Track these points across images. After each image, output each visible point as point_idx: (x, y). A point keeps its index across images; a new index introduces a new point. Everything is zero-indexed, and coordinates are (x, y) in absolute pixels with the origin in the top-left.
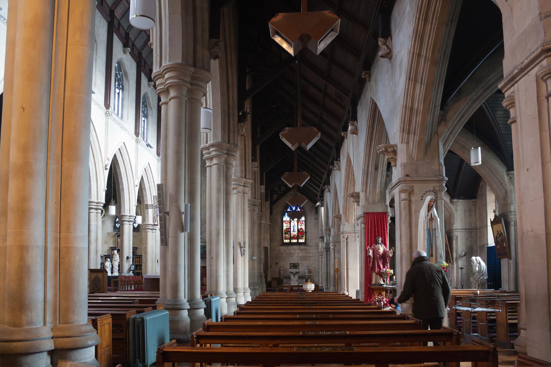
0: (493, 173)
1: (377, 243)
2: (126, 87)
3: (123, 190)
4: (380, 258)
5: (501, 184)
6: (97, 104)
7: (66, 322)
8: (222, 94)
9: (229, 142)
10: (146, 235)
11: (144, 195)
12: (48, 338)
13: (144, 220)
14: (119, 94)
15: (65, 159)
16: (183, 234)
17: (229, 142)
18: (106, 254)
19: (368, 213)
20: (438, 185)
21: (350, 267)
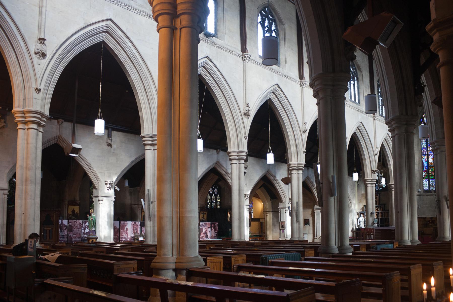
2: (360, 78)
3: (365, 159)
6: (31, 187)
7: (182, 256)
9: (407, 114)
11: (387, 161)
12: (171, 263)
13: (387, 181)
14: (354, 84)
15: (180, 170)
16: (333, 198)
17: (407, 114)
18: (361, 211)
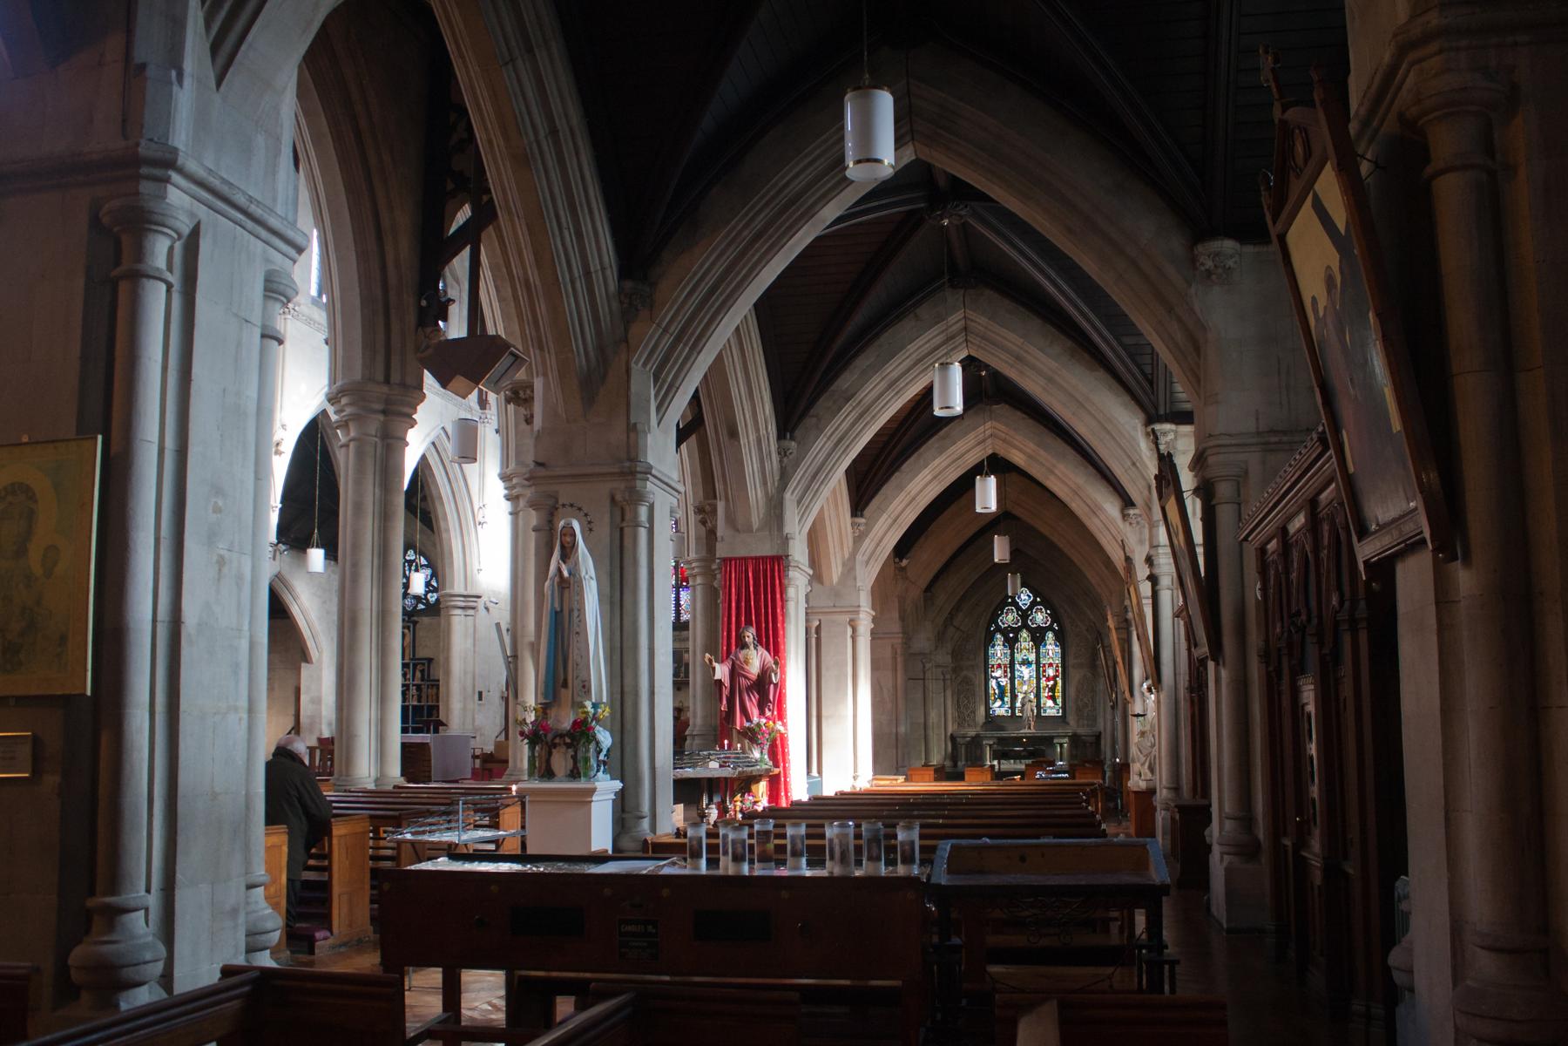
0: (1108, 432)
1: (743, 645)
4: (749, 689)
5: (1134, 464)
8: (362, 256)
9: (387, 381)
10: (449, 624)
17: (387, 381)
19: (731, 559)
20: (622, 486)
21: (824, 713)
